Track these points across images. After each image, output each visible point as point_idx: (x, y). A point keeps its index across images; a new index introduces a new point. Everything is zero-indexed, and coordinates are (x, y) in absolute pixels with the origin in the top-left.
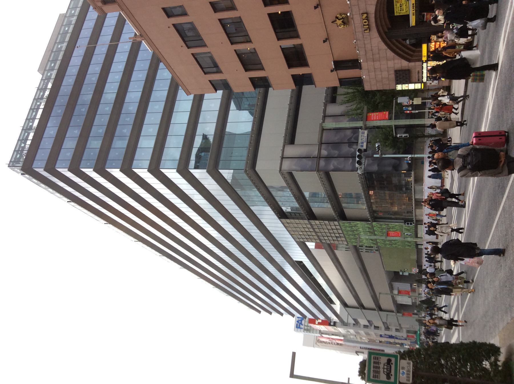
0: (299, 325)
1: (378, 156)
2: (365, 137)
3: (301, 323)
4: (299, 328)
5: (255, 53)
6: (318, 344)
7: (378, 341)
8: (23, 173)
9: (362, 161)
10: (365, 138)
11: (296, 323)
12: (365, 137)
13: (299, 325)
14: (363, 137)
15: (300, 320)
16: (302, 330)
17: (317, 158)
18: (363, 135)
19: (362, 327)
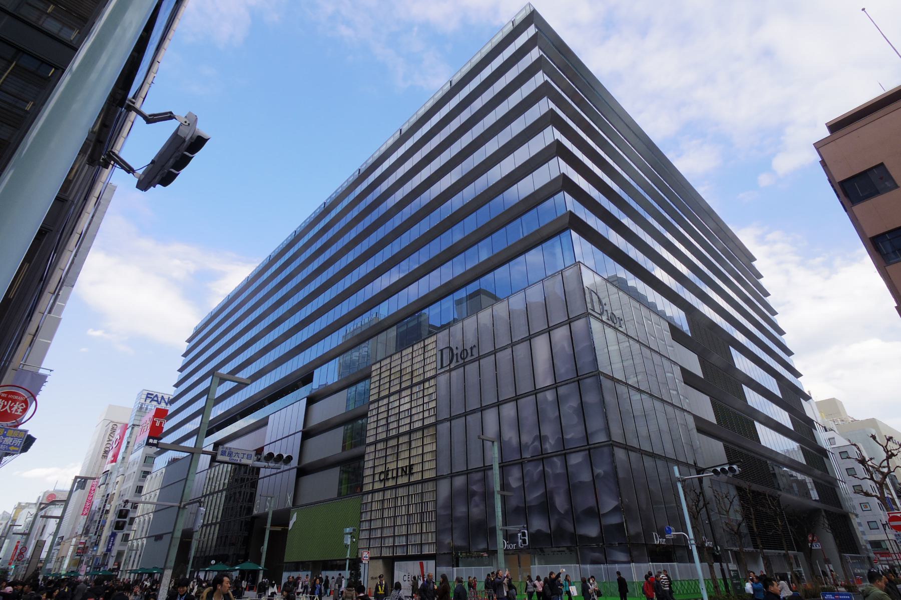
0: (151, 398)
1: (677, 474)
2: (240, 460)
3: (153, 400)
4: (147, 397)
5: (481, 308)
6: (111, 425)
7: (108, 508)
8: (403, 132)
9: (280, 463)
10: (239, 459)
11: (155, 394)
12: (240, 460)
13: (151, 398)
14: (241, 456)
15: (158, 399)
16: (143, 401)
17: (588, 444)
18: (246, 456)
19: (140, 484)
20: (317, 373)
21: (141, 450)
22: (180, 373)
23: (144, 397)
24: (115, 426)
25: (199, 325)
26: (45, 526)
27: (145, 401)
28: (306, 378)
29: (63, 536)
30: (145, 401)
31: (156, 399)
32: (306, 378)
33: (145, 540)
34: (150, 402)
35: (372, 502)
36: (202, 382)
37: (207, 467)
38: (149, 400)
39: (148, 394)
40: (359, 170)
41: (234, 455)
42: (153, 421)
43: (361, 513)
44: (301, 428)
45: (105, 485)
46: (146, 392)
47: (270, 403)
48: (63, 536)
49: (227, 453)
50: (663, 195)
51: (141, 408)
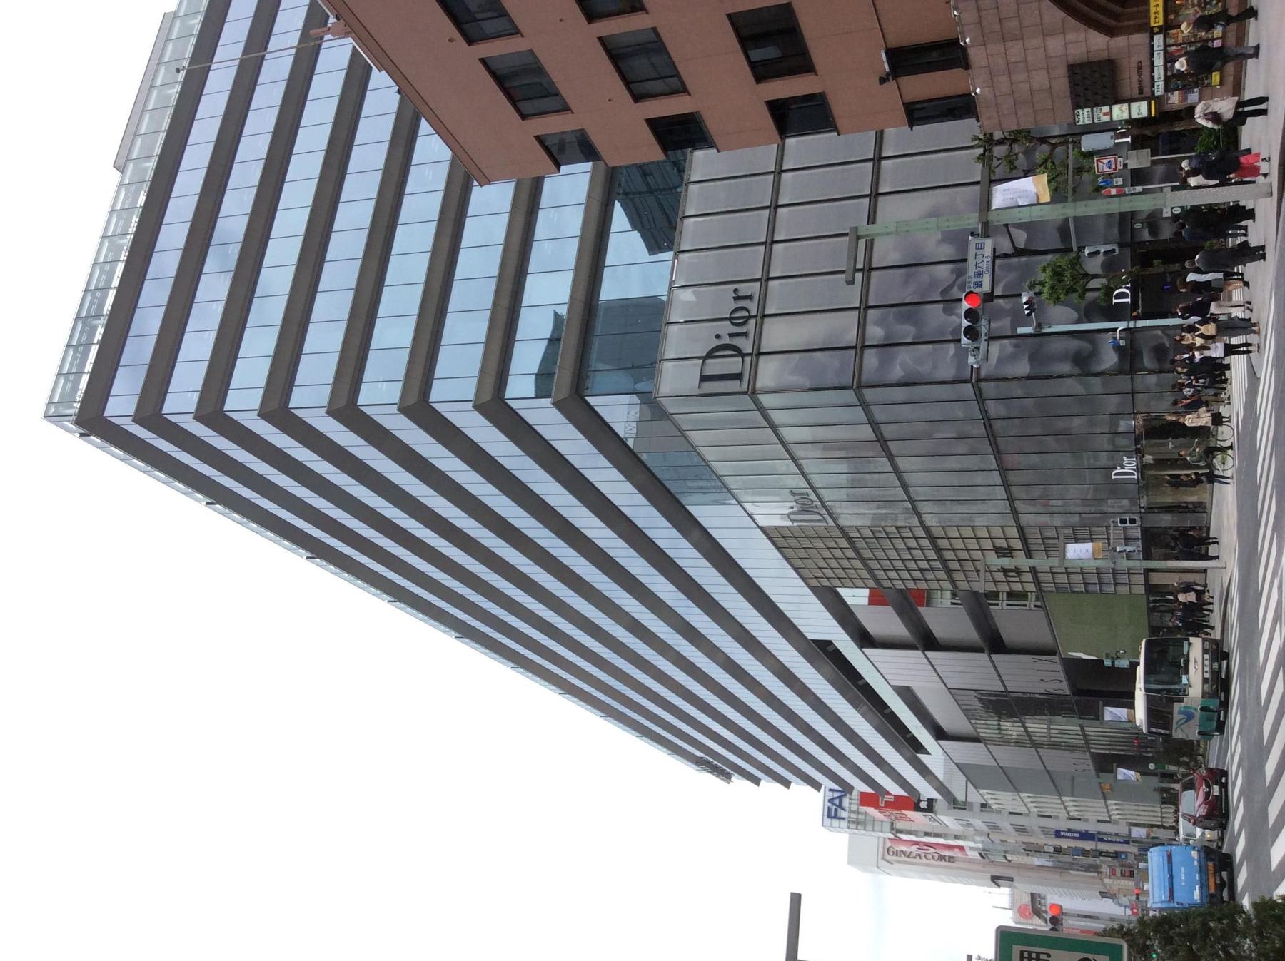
3: (840, 806)
4: (836, 817)
13: (836, 810)
14: (979, 259)
16: (844, 824)
18: (979, 252)
20: (813, 633)
21: (943, 818)
22: (792, 784)
23: (835, 822)
24: (891, 850)
25: (665, 752)
26: (1079, 916)
27: (843, 819)
28: (824, 653)
29: (1100, 892)
30: (843, 819)
31: (837, 802)
32: (824, 653)
33: (1109, 802)
34: (844, 810)
35: (1055, 583)
36: (699, 587)
37: (982, 745)
38: (843, 814)
39: (829, 816)
40: (308, 558)
41: (979, 269)
42: (885, 807)
43: (1073, 592)
44: (919, 653)
45: (1007, 855)
46: (828, 821)
47: (861, 677)
48: (1100, 892)
49: (978, 280)
50: (364, 55)
51: (857, 823)
